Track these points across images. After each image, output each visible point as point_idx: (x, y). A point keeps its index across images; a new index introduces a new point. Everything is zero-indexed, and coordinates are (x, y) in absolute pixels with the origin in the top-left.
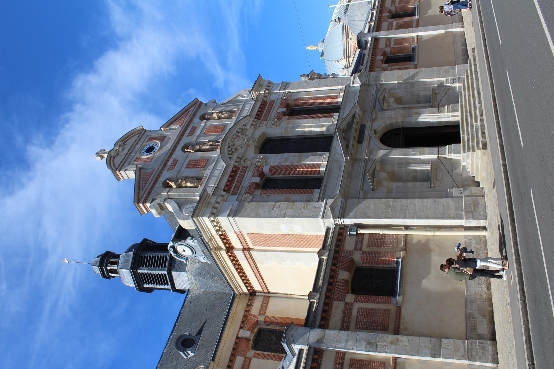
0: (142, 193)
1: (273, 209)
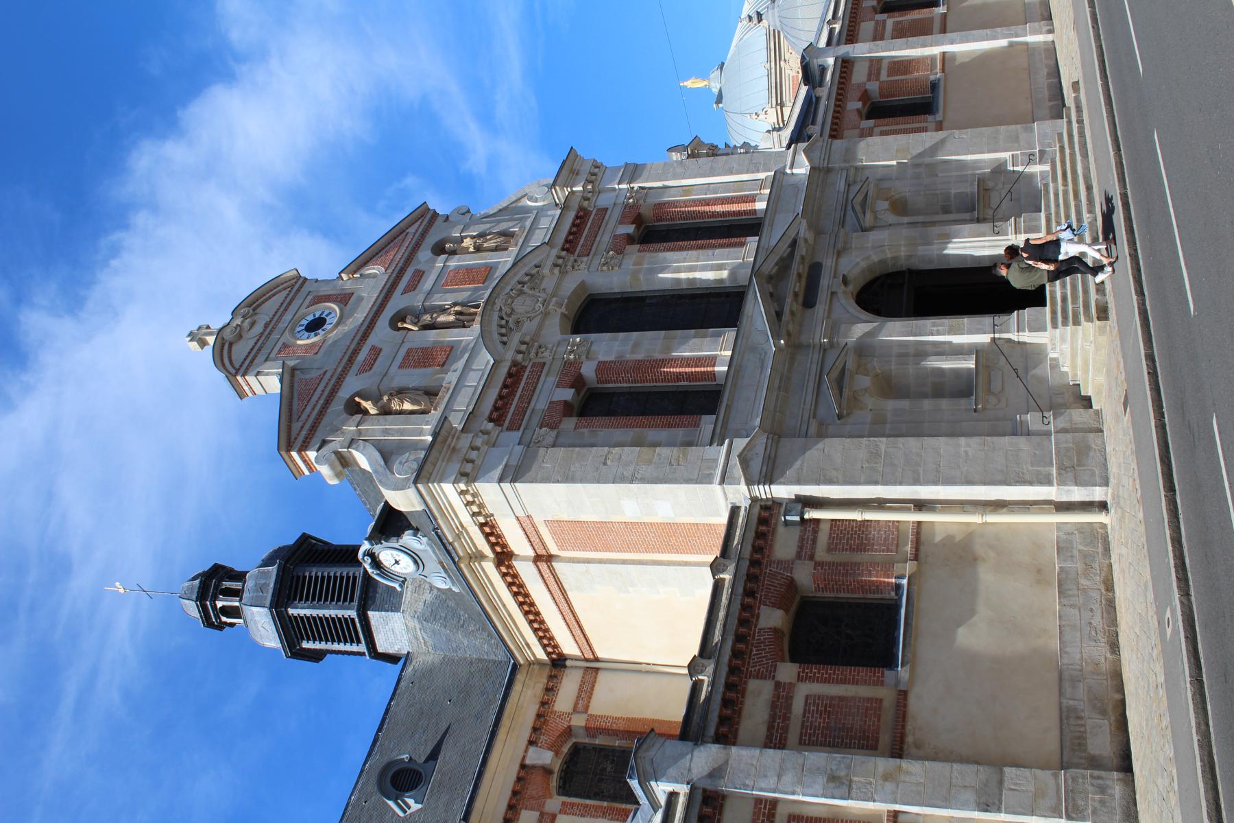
0: (296, 426)
1: (605, 464)
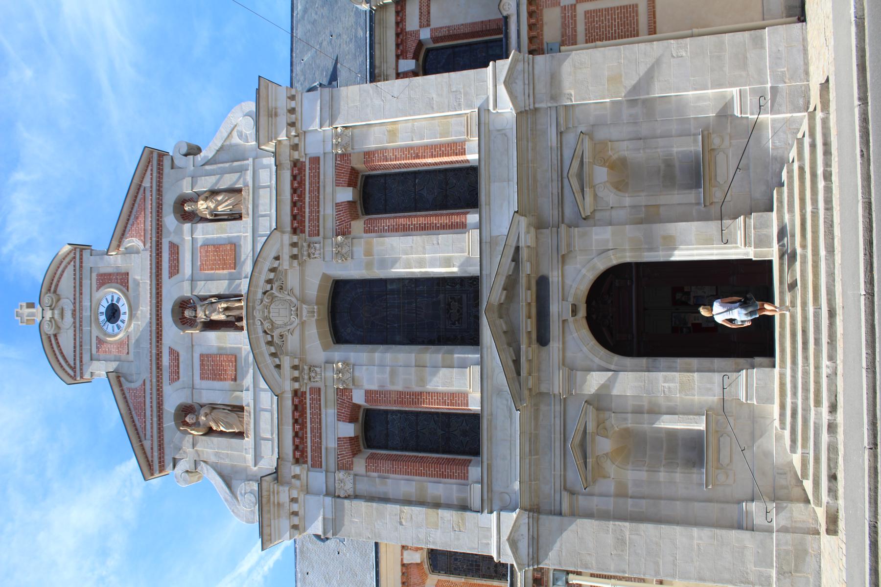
0: (147, 444)
1: (401, 524)
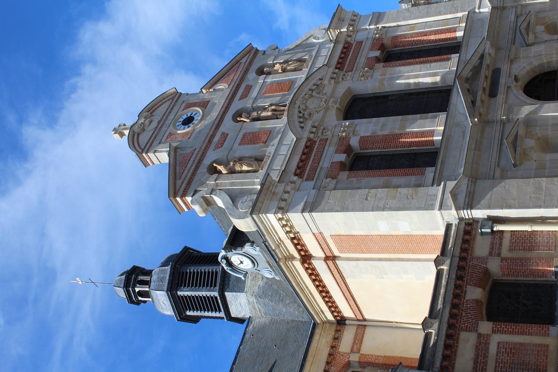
0: (179, 182)
1: (367, 199)
